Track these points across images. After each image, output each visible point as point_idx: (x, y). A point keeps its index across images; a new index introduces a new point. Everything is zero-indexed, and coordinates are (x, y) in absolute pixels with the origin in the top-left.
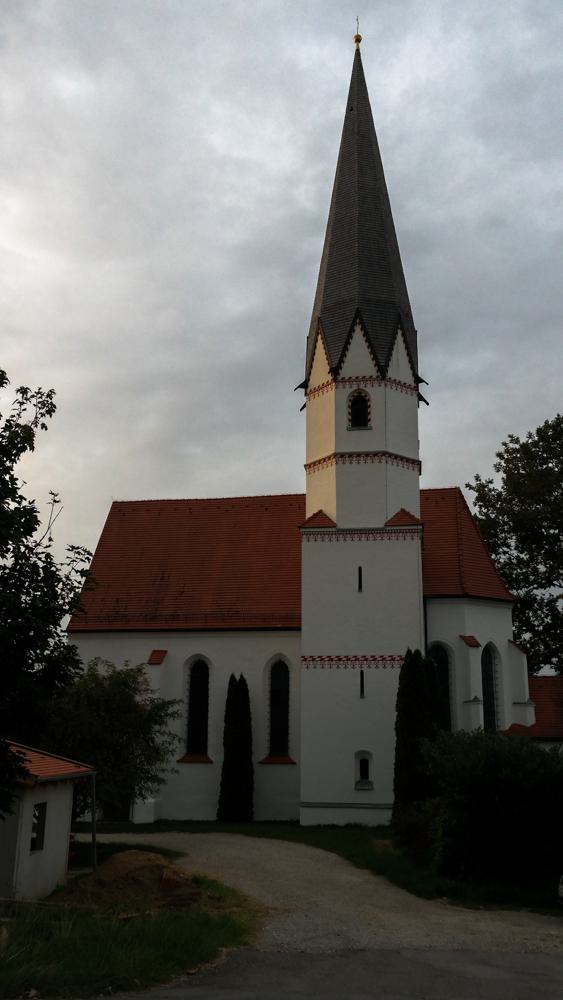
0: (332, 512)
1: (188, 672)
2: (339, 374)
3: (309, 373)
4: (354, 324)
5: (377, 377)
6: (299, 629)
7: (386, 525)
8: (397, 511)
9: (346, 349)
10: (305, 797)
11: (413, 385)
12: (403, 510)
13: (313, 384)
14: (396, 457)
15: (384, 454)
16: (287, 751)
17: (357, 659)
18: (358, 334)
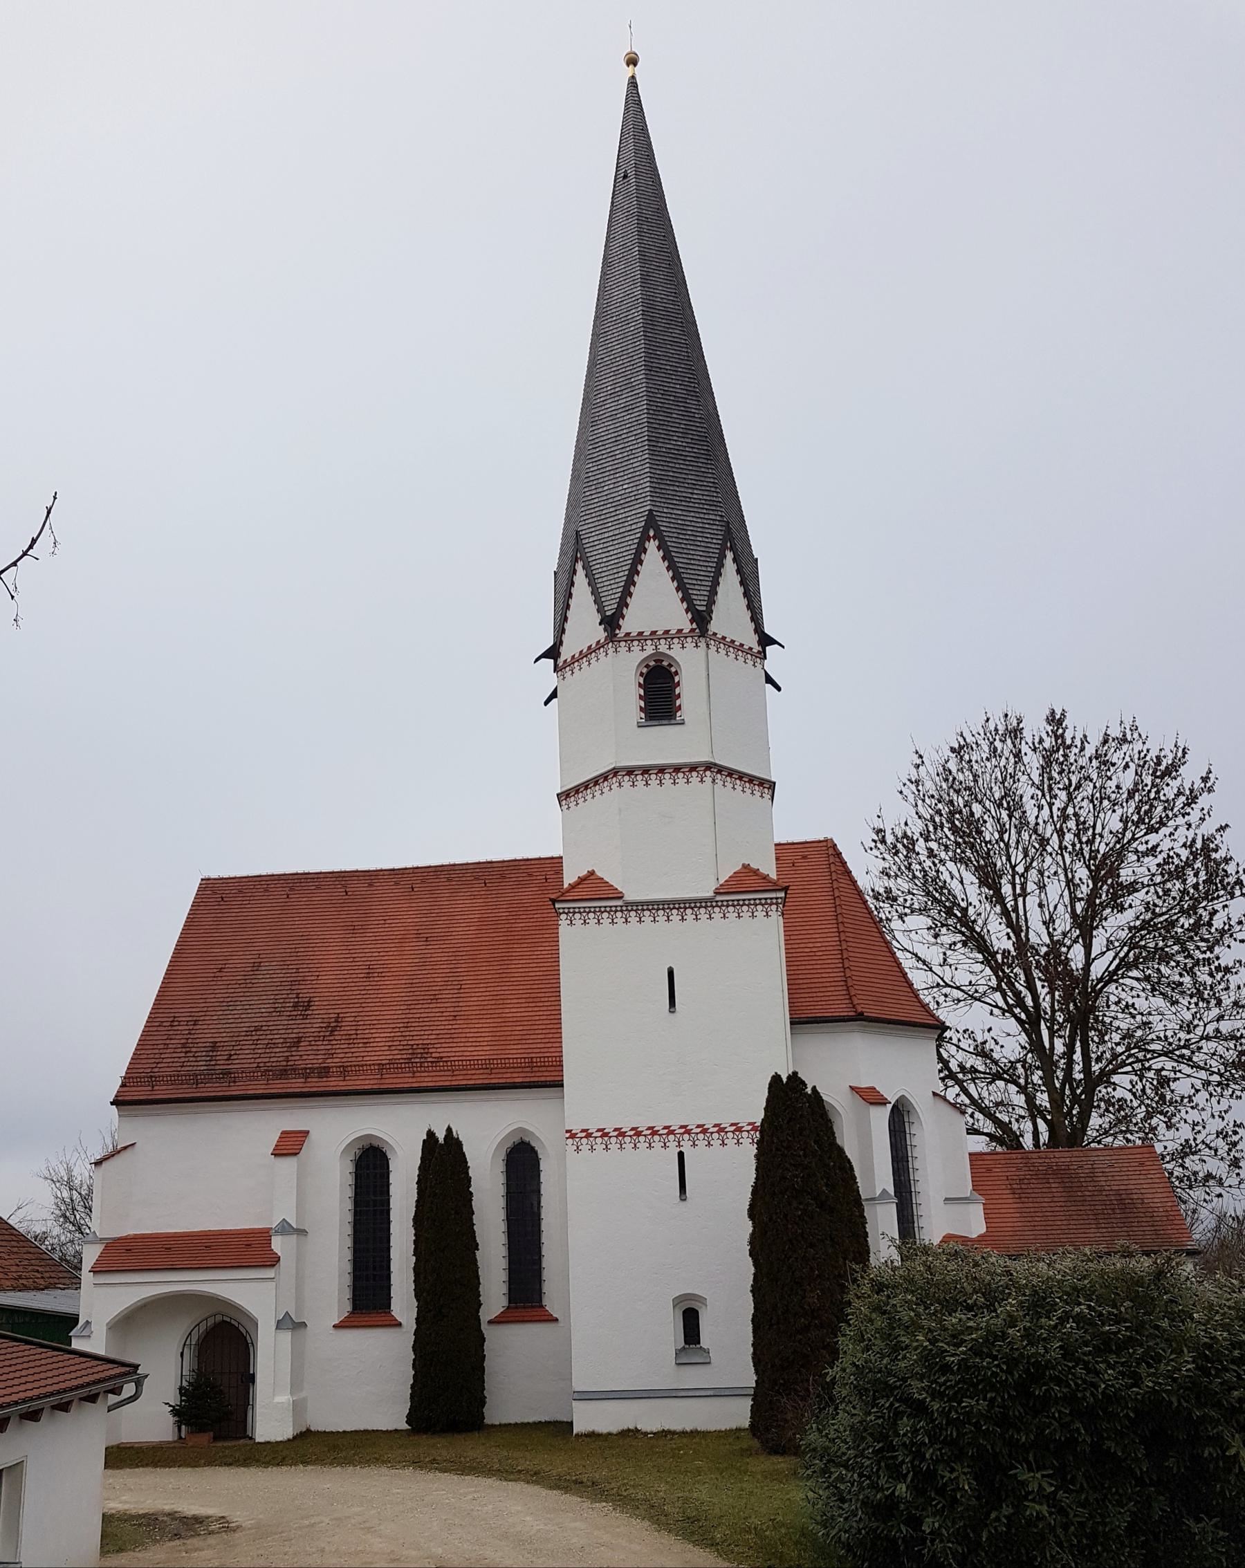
0: (611, 875)
1: (350, 1168)
2: (619, 627)
3: (560, 631)
4: (645, 537)
5: (692, 630)
6: (560, 1085)
7: (717, 893)
8: (738, 867)
9: (631, 581)
10: (579, 1385)
11: (757, 648)
12: (746, 867)
13: (566, 653)
14: (731, 773)
15: (709, 766)
16: (541, 1300)
17: (672, 1132)
18: (653, 554)
